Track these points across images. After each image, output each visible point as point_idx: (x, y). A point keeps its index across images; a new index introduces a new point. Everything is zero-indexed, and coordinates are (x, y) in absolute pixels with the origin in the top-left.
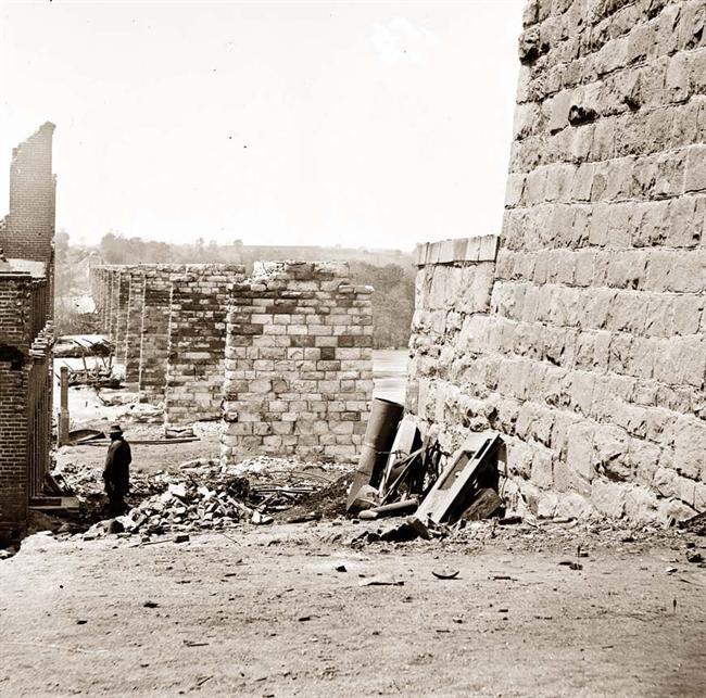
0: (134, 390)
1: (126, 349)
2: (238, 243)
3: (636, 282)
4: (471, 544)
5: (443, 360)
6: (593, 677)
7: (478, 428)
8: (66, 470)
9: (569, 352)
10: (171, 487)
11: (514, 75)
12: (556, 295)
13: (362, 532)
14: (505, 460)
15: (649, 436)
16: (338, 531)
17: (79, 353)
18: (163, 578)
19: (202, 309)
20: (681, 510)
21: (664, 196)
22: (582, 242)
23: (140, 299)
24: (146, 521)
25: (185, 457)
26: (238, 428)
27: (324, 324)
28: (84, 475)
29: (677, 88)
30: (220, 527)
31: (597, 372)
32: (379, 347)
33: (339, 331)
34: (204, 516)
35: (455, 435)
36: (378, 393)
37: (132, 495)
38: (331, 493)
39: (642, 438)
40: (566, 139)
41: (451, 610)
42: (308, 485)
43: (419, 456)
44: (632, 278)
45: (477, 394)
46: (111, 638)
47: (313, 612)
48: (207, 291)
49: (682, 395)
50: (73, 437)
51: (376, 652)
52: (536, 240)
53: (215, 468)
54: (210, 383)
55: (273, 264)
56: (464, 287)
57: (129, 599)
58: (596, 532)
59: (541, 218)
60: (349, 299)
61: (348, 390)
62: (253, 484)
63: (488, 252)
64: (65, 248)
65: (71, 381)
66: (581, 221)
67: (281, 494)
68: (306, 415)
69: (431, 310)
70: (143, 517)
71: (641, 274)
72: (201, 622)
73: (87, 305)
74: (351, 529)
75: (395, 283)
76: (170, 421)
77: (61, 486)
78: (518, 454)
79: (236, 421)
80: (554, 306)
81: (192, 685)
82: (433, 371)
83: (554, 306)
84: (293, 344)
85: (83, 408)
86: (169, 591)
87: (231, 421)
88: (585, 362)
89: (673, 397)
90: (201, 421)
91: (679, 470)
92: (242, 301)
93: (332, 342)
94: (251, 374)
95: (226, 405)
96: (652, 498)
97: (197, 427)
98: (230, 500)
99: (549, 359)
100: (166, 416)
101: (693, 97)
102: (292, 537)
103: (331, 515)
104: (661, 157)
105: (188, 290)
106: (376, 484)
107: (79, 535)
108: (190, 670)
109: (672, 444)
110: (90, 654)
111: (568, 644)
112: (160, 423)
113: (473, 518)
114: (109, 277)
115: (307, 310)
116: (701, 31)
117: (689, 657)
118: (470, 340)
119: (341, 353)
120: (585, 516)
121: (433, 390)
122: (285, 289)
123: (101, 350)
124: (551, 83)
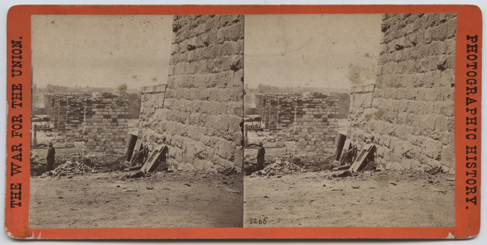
0: (267, 131)
1: (265, 119)
2: (299, 87)
3: (415, 98)
4: (158, 179)
5: (358, 122)
6: (397, 218)
7: (368, 143)
8: (35, 156)
9: (187, 120)
10: (277, 161)
11: (171, 36)
12: (183, 102)
13: (125, 175)
14: (376, 152)
15: (211, 146)
16: (118, 175)
17: (40, 120)
18: (270, 189)
19: (288, 107)
20: (221, 168)
21: (423, 72)
22: (192, 86)
23: (58, 104)
24: (269, 171)
25: (71, 152)
26: (298, 143)
27: (324, 111)
28: (41, 158)
29: (427, 39)
30: (291, 173)
31: (195, 126)
32: (341, 118)
33: (118, 113)
34: (286, 170)
35: (362, 145)
36: (129, 133)
37: (56, 164)
38: (325, 163)
39: (416, 145)
40: (187, 55)
41: (152, 199)
42: (108, 161)
43: (142, 152)
44: (414, 96)
45: (160, 133)
46: (254, 207)
47: (110, 199)
48: (289, 101)
49: (221, 133)
50: (38, 146)
51: (333, 211)
52: (385, 85)
53: (291, 155)
54: (79, 129)
55: (309, 93)
56: (156, 100)
57: (260, 195)
58: (195, 175)
59: (179, 79)
60: (331, 104)
61: (121, 132)
62: (92, 161)
63: (371, 89)
64: (36, 88)
65: (37, 129)
66: (191, 80)
67: (100, 163)
68: (108, 139)
69: (146, 107)
70: (268, 170)
71: (416, 95)
72: (76, 203)
73: (42, 105)
74: (122, 174)
75: (135, 99)
76: (278, 141)
77: (34, 161)
78: (380, 150)
79: (297, 141)
80: (183, 106)
81: (73, 222)
82: (146, 126)
83: (183, 106)
84: (315, 117)
85: (41, 137)
86: (273, 193)
87: (296, 141)
88: (192, 123)
89: (219, 133)
90: (77, 141)
91: (427, 155)
92: (89, 104)
93: (116, 117)
94: (302, 127)
95: (295, 136)
96: (212, 164)
97: (286, 143)
98: (85, 165)
99: (181, 122)
100: (66, 140)
101: (225, 42)
102: (104, 177)
103: (325, 169)
104: (422, 60)
105: (284, 101)
106: (129, 161)
107: (39, 176)
108: (73, 217)
109: (218, 148)
110: (42, 213)
111: (187, 209)
112: (64, 142)
113: (158, 171)
114: (49, 97)
115: (319, 107)
116: (435, 21)
117: (426, 212)
118: (157, 116)
119: (329, 120)
120: (399, 169)
121: (146, 132)
122: (312, 101)
123: (46, 120)
124: (391, 37)
